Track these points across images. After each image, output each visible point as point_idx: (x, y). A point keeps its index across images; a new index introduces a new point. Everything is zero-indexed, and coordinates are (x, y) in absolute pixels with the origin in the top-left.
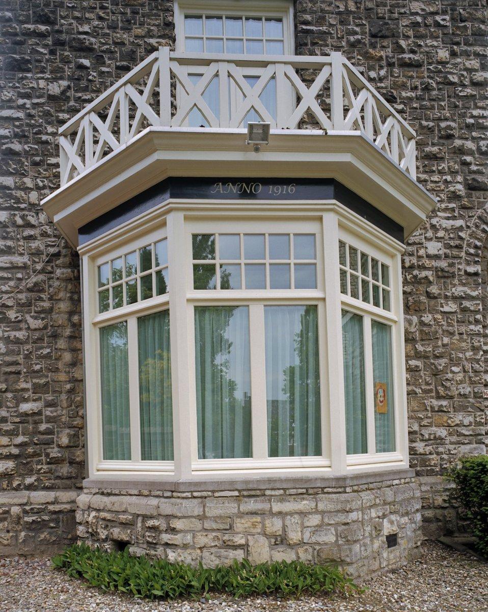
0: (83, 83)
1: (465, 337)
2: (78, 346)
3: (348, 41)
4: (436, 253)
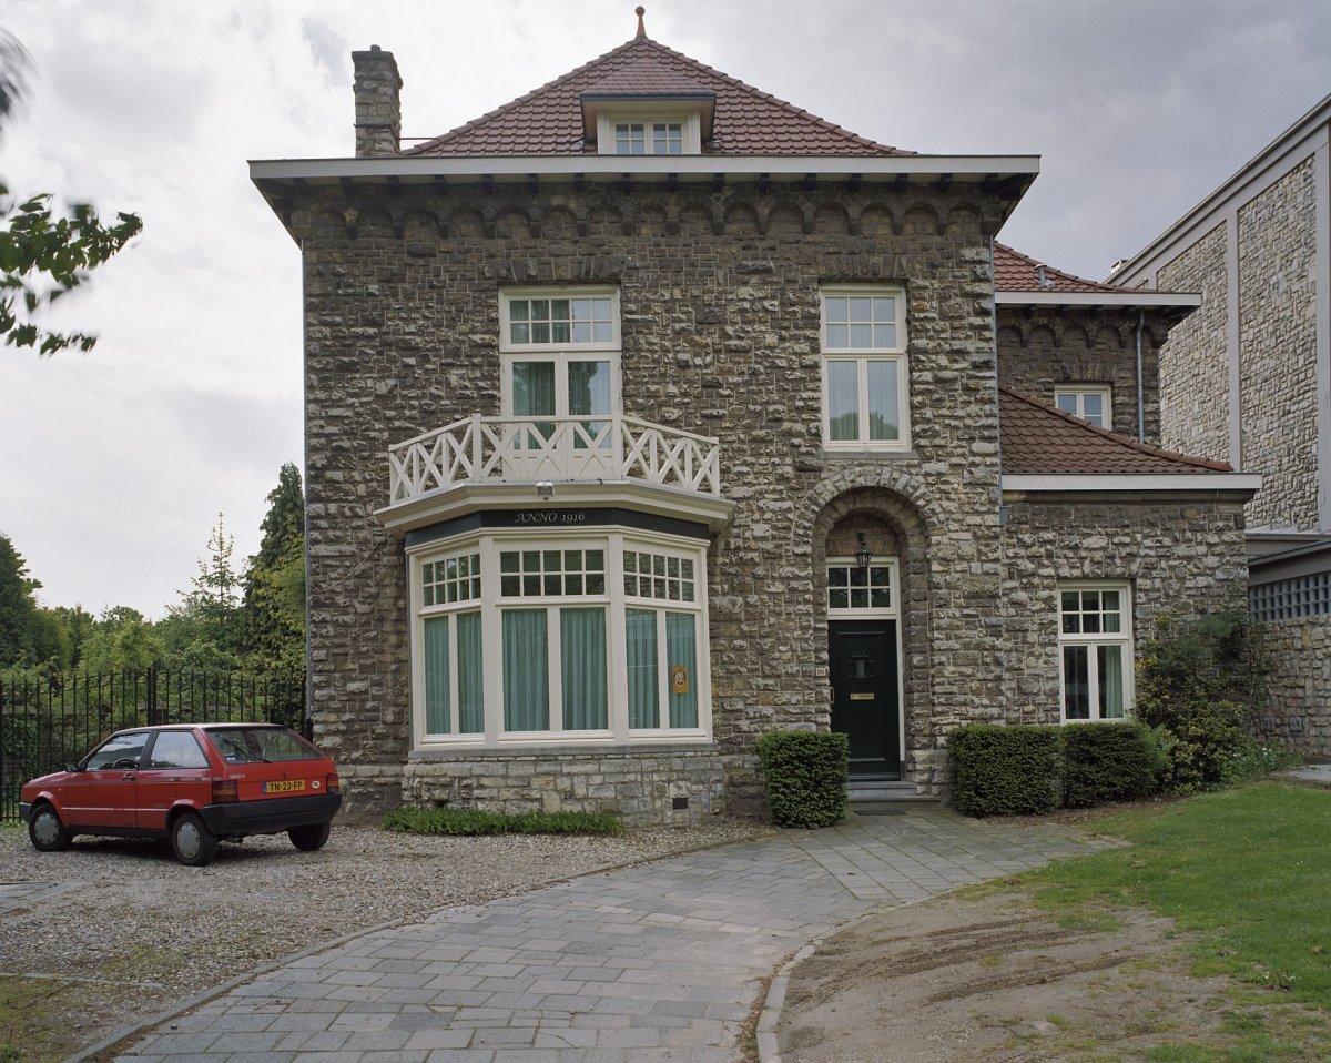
0: (409, 381)
1: (793, 616)
2: (403, 628)
3: (673, 329)
4: (763, 534)
